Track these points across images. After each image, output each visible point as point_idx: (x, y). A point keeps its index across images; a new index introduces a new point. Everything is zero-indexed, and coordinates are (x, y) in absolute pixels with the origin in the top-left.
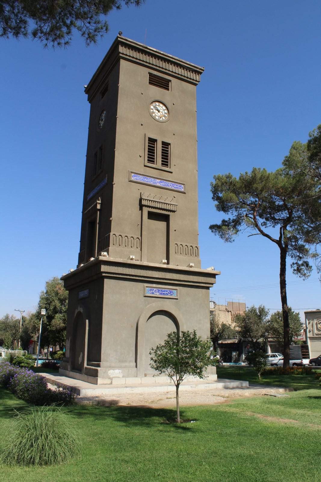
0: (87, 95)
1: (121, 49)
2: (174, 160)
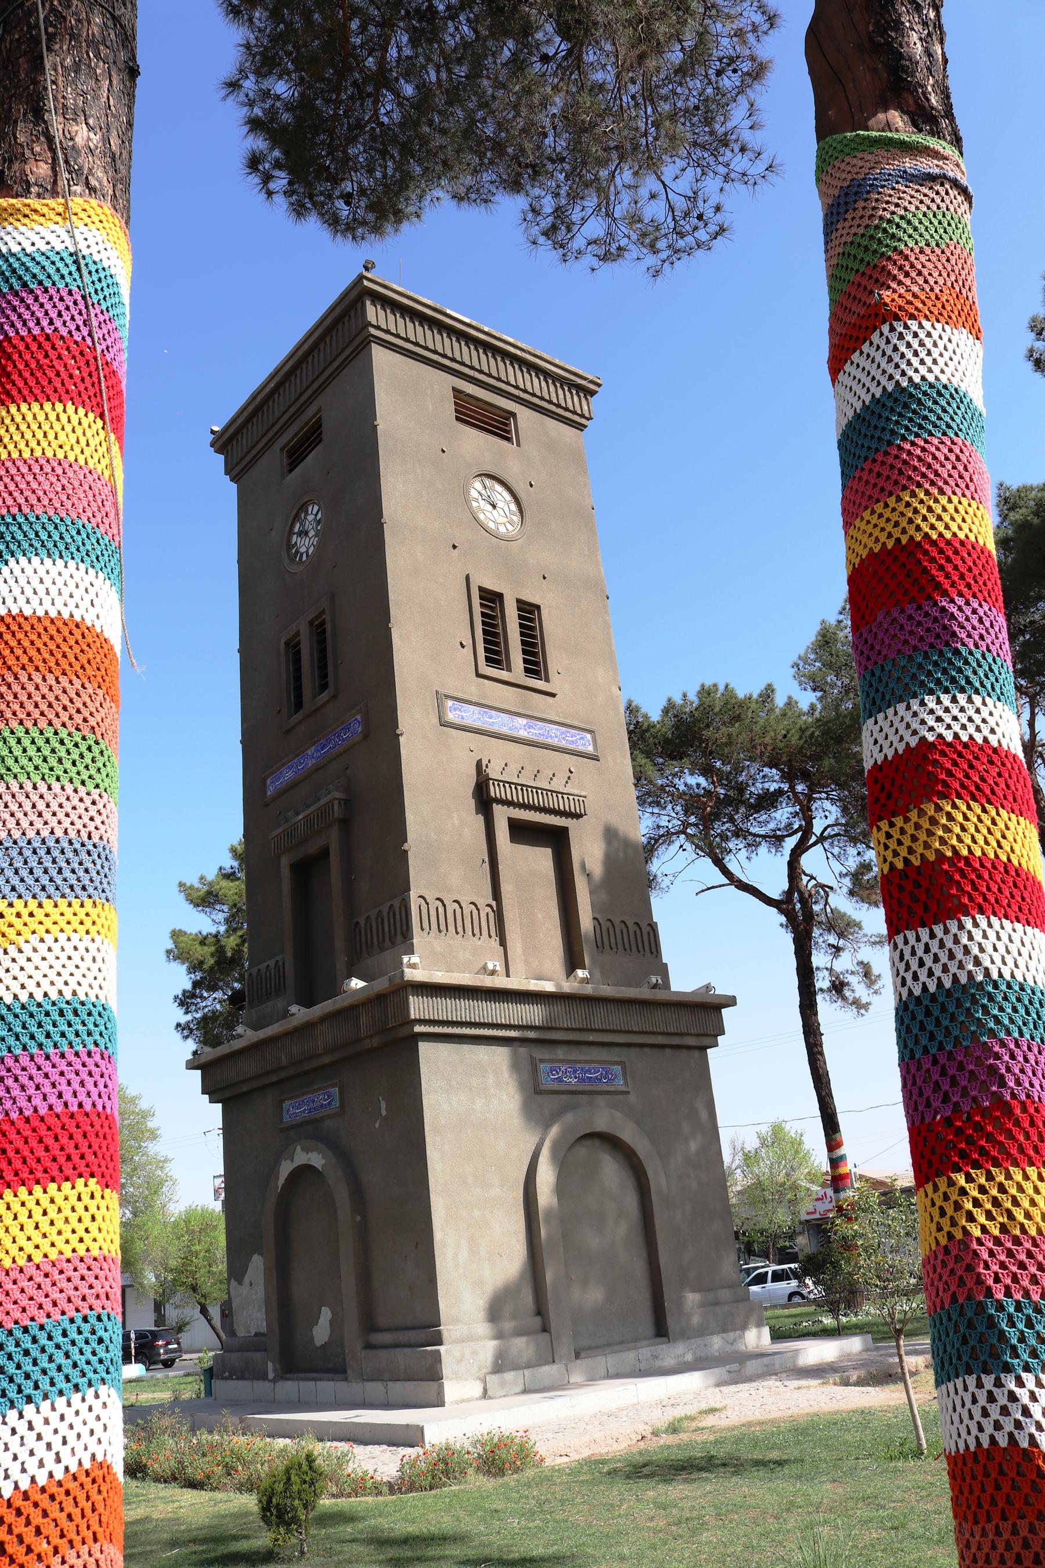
0: (221, 458)
1: (373, 313)
2: (555, 658)
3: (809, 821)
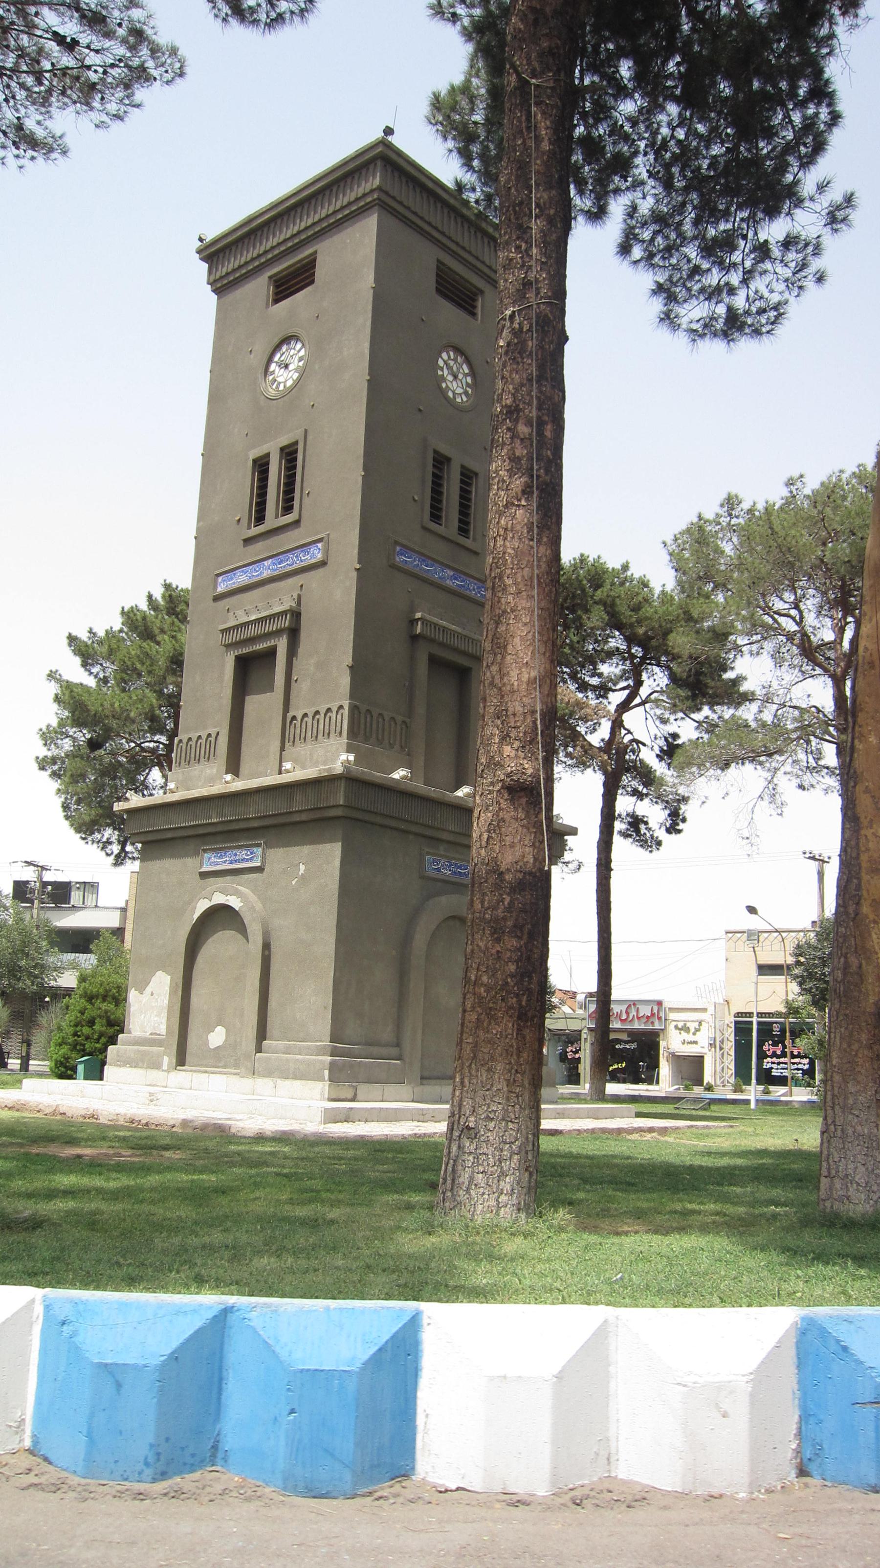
3: (639, 683)
